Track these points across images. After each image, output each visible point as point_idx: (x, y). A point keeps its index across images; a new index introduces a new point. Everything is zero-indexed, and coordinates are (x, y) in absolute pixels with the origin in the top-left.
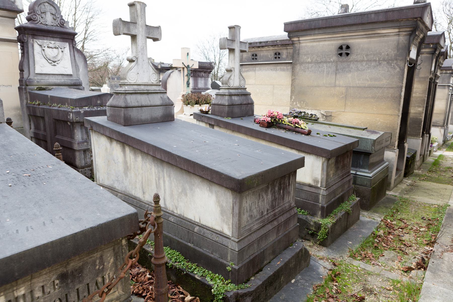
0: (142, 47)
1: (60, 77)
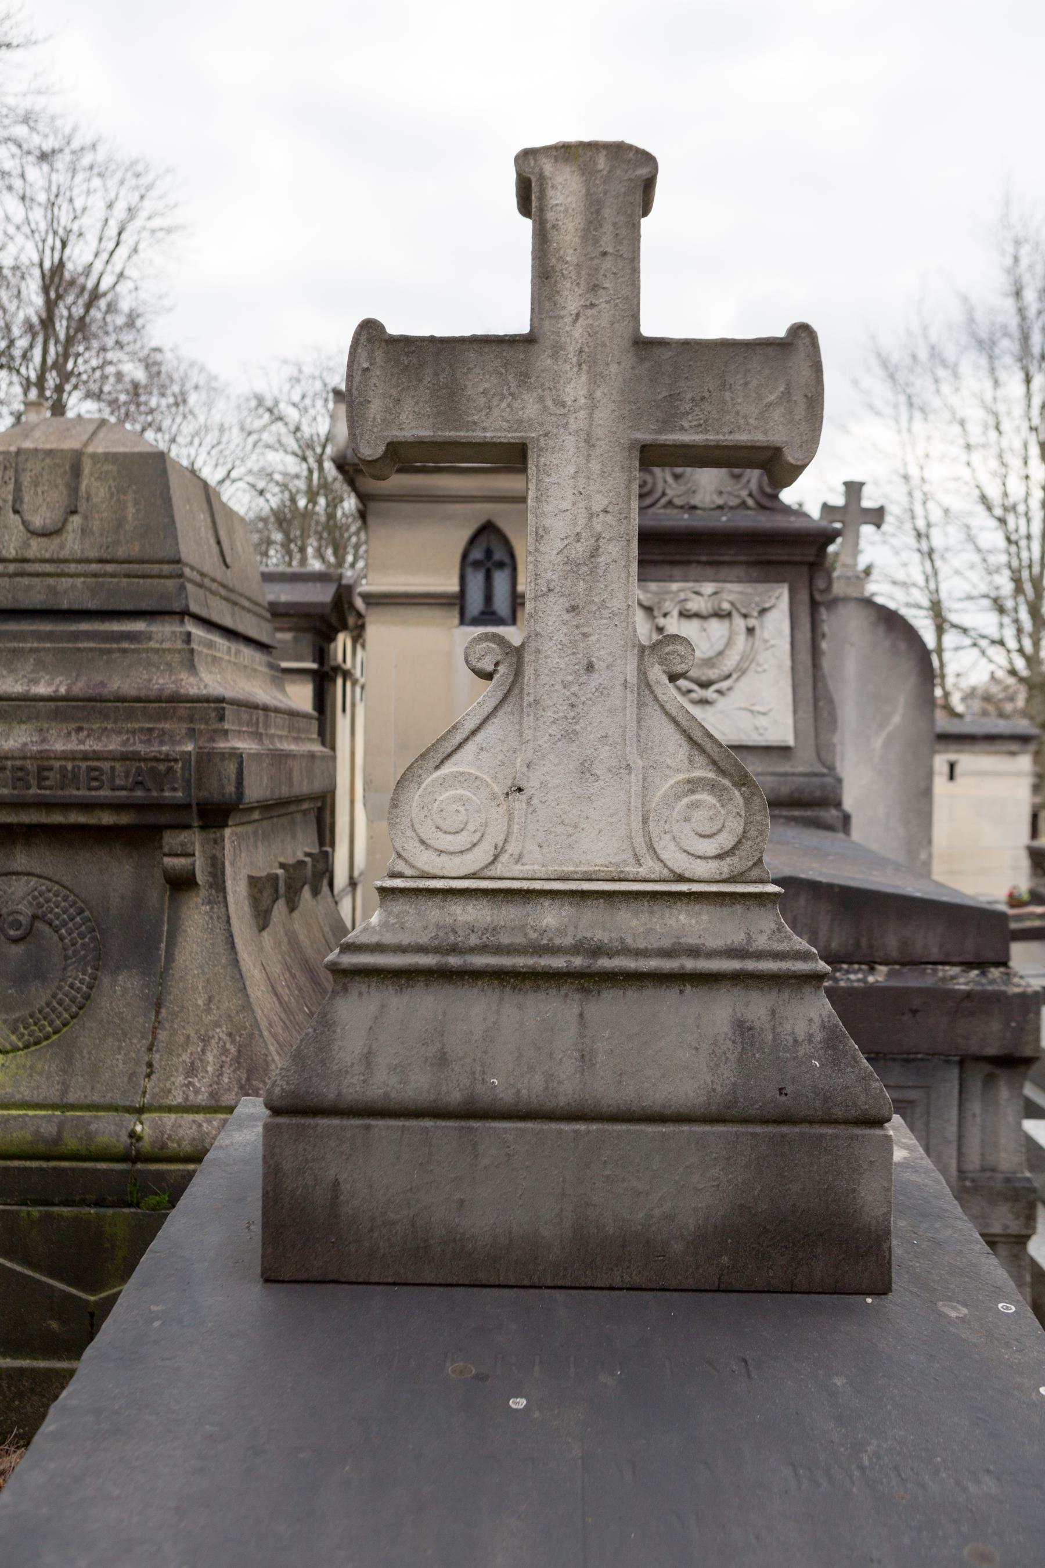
0: (579, 550)
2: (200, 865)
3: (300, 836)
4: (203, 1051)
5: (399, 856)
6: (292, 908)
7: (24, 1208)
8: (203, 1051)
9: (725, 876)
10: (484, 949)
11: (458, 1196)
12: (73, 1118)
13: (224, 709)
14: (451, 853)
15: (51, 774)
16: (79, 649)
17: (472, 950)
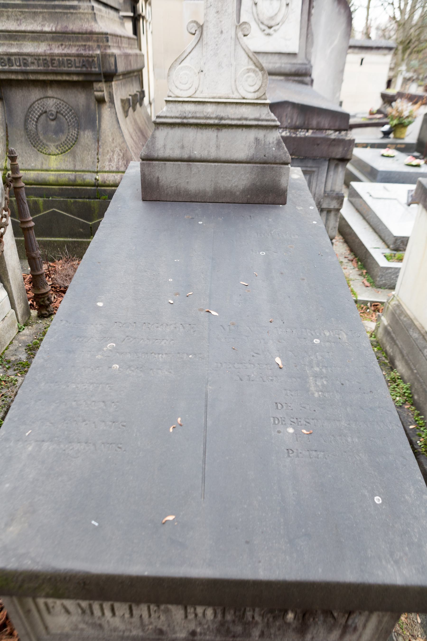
1: (276, 58)
2: (106, 94)
3: (135, 85)
4: (113, 155)
5: (170, 91)
6: (134, 110)
7: (69, 200)
8: (113, 155)
9: (256, 98)
10: (192, 118)
11: (187, 181)
12: (78, 174)
13: (108, 37)
14: (184, 90)
15: (55, 62)
16: (56, 12)
17: (190, 118)
